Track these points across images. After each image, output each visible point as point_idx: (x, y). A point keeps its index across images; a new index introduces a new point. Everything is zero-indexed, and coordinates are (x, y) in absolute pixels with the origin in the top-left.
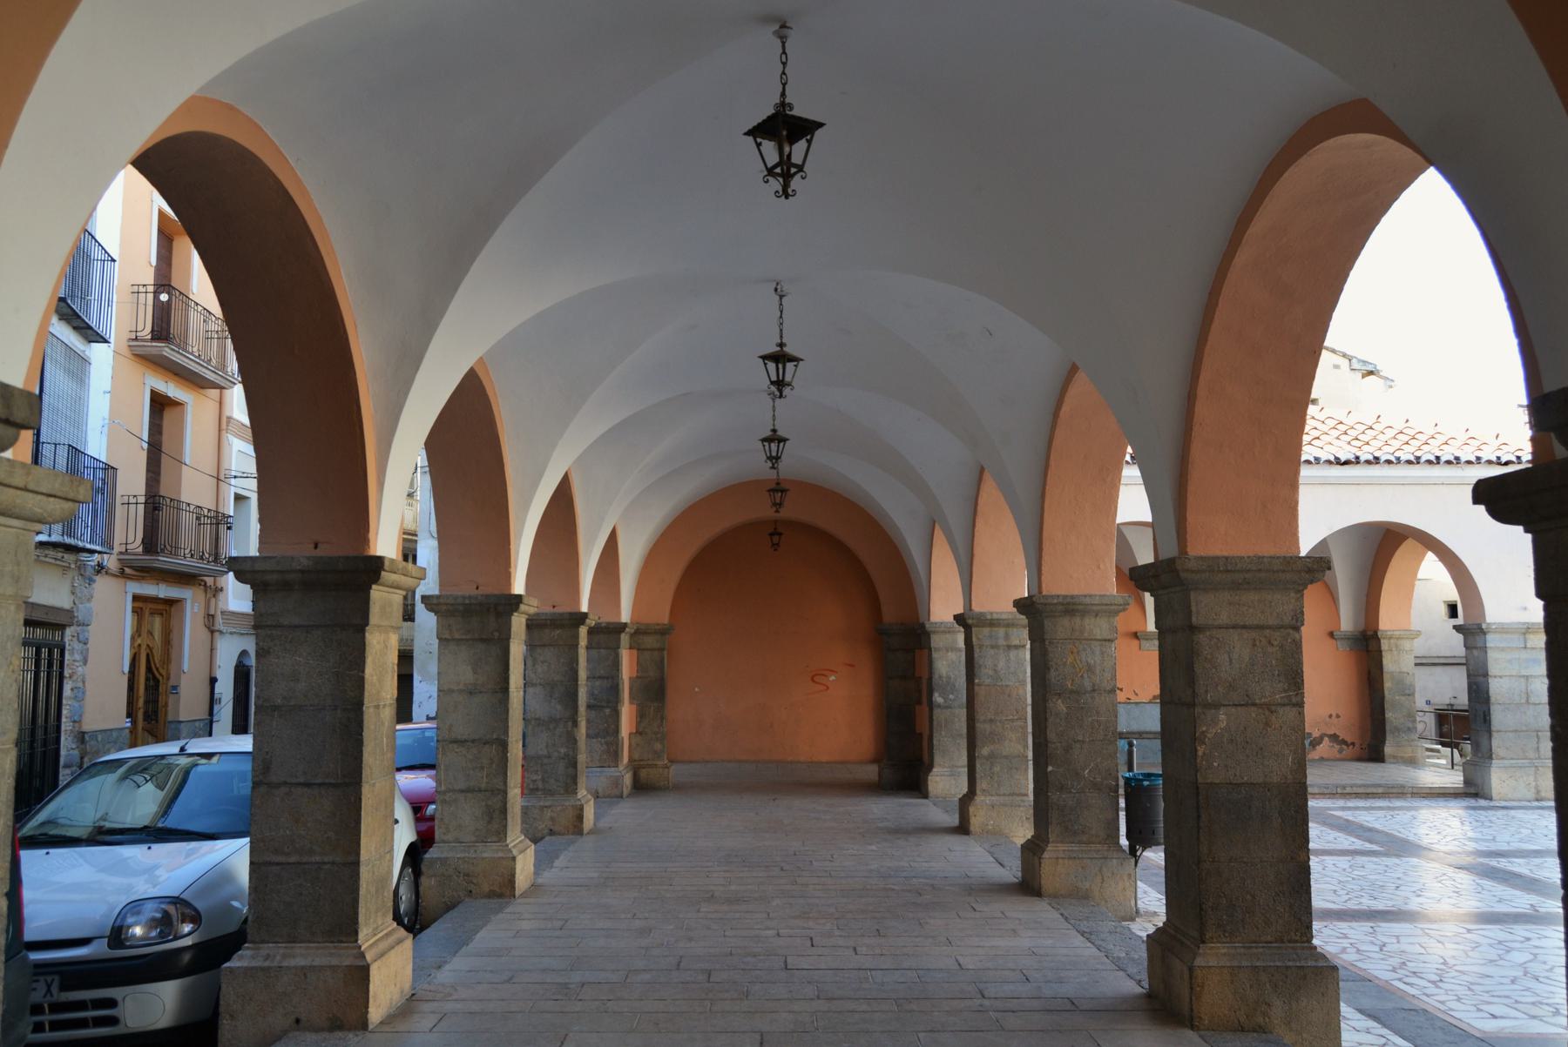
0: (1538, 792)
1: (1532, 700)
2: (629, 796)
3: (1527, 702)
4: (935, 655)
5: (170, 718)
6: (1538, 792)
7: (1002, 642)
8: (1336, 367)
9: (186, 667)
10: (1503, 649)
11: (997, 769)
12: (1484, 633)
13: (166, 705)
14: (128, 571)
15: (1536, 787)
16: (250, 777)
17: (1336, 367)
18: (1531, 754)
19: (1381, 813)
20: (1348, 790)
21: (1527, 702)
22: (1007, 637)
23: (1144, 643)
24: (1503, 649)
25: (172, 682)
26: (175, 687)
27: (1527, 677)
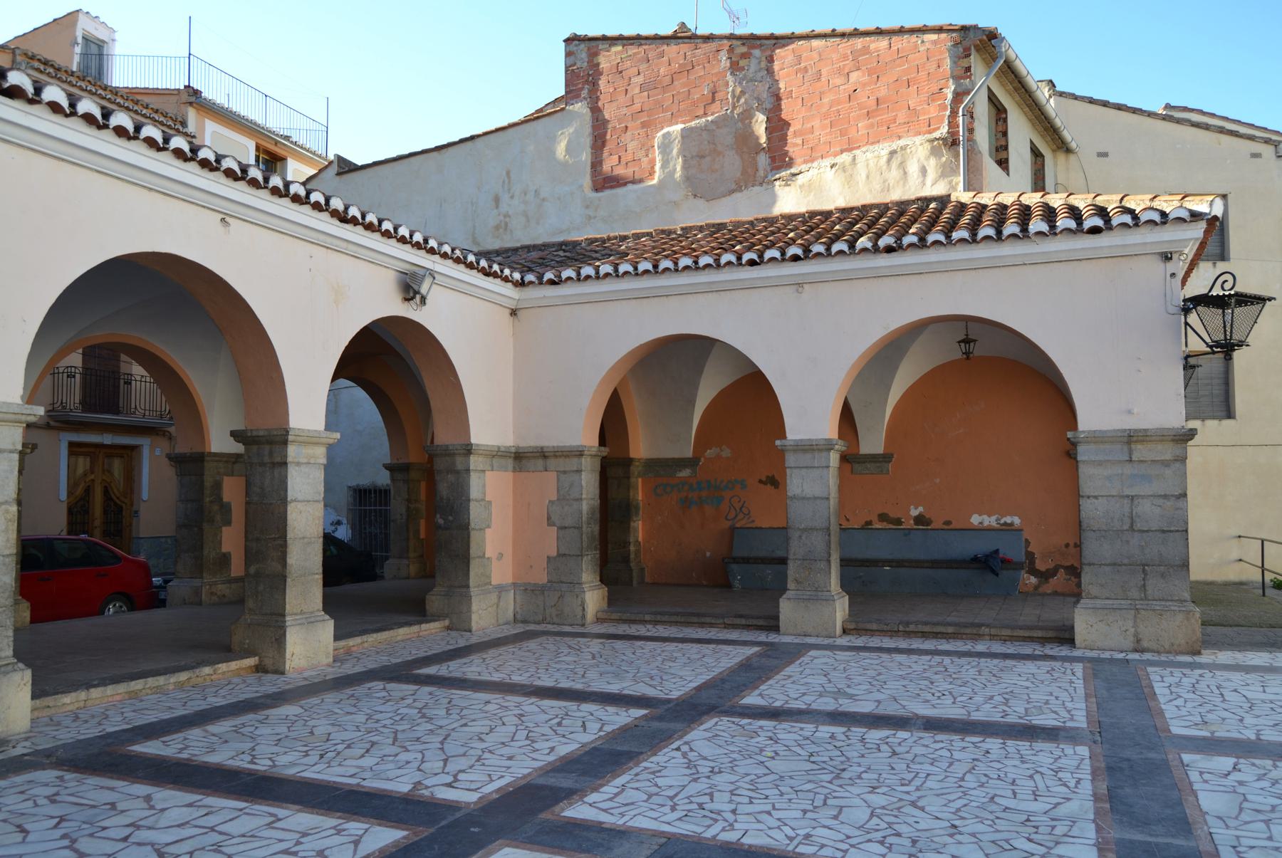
0: (1138, 641)
1: (1138, 526)
2: (541, 618)
3: (1132, 528)
4: (438, 478)
5: (134, 535)
6: (1138, 641)
7: (266, 459)
8: (1256, 155)
9: (145, 496)
10: (1100, 463)
11: (261, 588)
12: (285, 443)
13: (131, 525)
14: (52, 423)
15: (1136, 635)
16: (473, 591)
17: (1256, 155)
18: (1135, 593)
19: (1030, 667)
20: (912, 628)
21: (1132, 528)
22: (271, 453)
23: (856, 466)
24: (1100, 463)
25: (135, 508)
26: (136, 512)
27: (1132, 498)
